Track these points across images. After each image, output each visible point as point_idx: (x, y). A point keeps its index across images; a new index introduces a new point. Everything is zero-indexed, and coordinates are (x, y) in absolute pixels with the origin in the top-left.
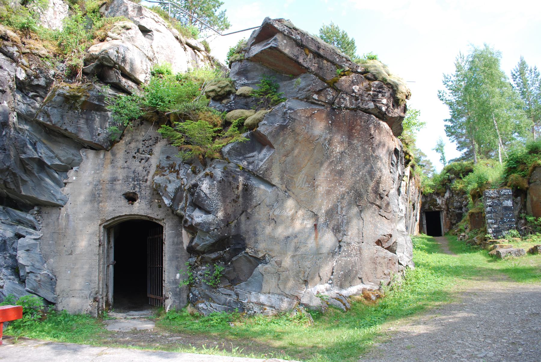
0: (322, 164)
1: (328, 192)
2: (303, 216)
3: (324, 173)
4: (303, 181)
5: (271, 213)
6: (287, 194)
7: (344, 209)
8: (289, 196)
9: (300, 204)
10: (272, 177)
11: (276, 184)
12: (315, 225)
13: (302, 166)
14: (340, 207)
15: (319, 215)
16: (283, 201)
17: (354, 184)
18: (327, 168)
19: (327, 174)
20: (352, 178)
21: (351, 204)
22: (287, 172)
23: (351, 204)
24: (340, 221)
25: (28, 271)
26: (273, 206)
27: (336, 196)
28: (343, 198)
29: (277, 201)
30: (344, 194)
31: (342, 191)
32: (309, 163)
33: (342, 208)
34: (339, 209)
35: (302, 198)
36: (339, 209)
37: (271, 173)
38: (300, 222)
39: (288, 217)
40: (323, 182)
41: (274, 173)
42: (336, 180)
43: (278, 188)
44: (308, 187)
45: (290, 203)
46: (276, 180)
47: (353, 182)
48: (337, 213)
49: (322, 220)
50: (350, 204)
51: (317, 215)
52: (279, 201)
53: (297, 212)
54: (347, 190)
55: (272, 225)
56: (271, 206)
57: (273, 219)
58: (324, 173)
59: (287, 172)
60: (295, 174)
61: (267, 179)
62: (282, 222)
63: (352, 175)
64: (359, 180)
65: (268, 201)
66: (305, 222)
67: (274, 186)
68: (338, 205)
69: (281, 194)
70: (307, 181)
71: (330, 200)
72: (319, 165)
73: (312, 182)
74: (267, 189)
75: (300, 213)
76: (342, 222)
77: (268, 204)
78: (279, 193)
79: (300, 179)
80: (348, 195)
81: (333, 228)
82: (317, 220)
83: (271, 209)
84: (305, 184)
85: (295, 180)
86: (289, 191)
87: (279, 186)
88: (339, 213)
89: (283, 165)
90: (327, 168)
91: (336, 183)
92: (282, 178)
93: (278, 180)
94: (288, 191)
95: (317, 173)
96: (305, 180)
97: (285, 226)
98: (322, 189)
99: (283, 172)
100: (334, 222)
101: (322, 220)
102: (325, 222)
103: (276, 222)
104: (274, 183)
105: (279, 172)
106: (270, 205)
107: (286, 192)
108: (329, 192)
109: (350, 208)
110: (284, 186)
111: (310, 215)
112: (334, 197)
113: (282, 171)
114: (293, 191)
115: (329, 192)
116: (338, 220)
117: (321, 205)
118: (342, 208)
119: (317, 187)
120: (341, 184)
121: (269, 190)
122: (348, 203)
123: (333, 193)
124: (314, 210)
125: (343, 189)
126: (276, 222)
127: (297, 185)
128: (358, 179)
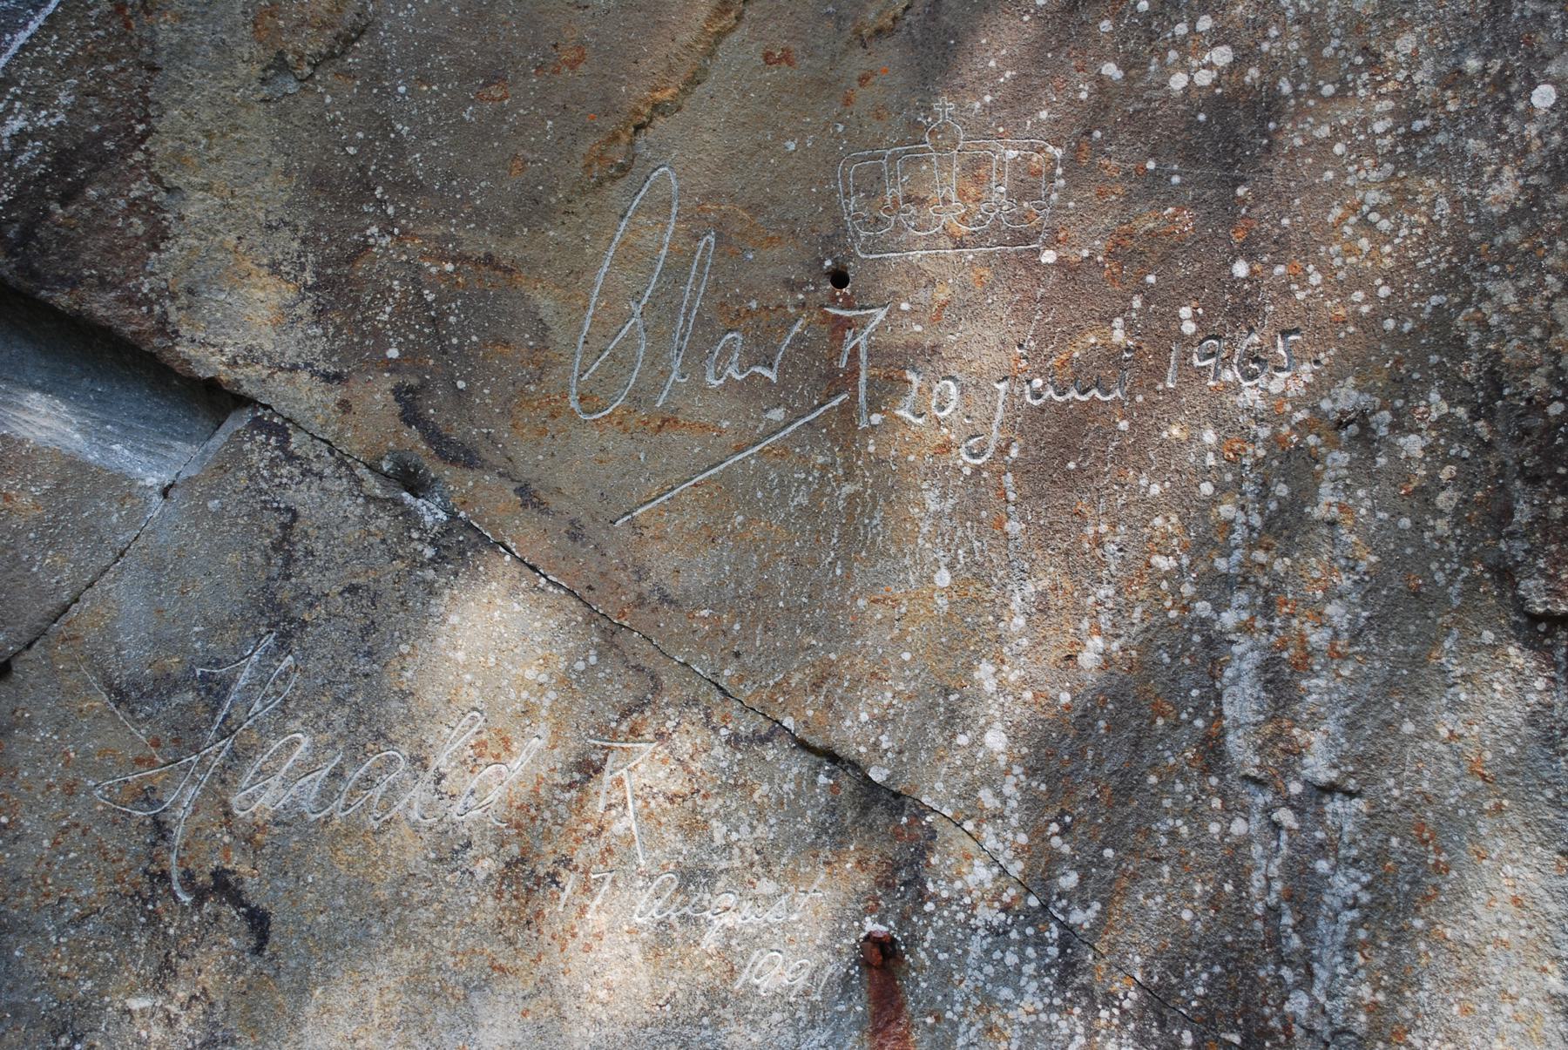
0: (935, 50)
1: (1061, 451)
2: (693, 827)
3: (975, 169)
4: (664, 307)
5: (183, 801)
6: (431, 513)
7: (1316, 687)
8: (462, 546)
9: (630, 652)
10: (166, 266)
11: (248, 379)
12: (881, 962)
13: (634, 94)
14: (1245, 657)
15: (936, 794)
16: (379, 623)
17: (1450, 280)
18: (1019, 99)
19: (1026, 187)
20: (1403, 199)
21: (1421, 599)
22: (408, 187)
23: (1421, 599)
24: (1266, 877)
25: (1325, 775)
26: (214, 689)
27: (1182, 498)
28: (1286, 526)
29: (286, 629)
30: (1296, 464)
31: (1273, 415)
32: (741, 49)
33: (1280, 681)
34: (1242, 702)
35: (663, 563)
36: (1242, 702)
37: (149, 209)
38: (645, 908)
39: (451, 850)
40: (969, 309)
41: (196, 207)
42: (1165, 249)
43: (280, 430)
44: (751, 390)
45: (491, 640)
46: (246, 320)
47: (1436, 260)
48: (1212, 752)
49: (976, 871)
50: (1401, 606)
51: (896, 800)
52: (325, 629)
53: (588, 769)
54: (1347, 396)
55: (209, 968)
56: (188, 703)
57: (224, 886)
58: (975, 169)
59: (408, 187)
60: (534, 208)
61: (101, 306)
62: (372, 918)
63: (1414, 149)
64: (1528, 209)
65: (125, 618)
66: (728, 913)
67: (215, 400)
68: (1215, 644)
69: (329, 506)
70: (726, 312)
71: (1081, 567)
72: (889, 55)
73: (810, 324)
74: (122, 455)
75: (643, 772)
76: (1303, 891)
77: (133, 654)
78: (302, 496)
79: (618, 281)
80: (1363, 471)
81: (1158, 1001)
82: (904, 877)
83: (185, 737)
84: (697, 355)
85: (545, 302)
86: (466, 458)
87: (303, 397)
88: (1241, 750)
89: (332, 95)
90: (1019, 99)
91: (1163, 301)
92: (335, 289)
93: (285, 319)
94: (440, 472)
95: (871, 186)
96: (693, 294)
97: (415, 983)
98: (963, 398)
99: (339, 194)
100: (1167, 906)
101: (976, 871)
102: (1033, 910)
103: (259, 922)
104: (212, 364)
105: (271, 193)
106: (166, 685)
107: (411, 480)
108: (1065, 446)
109: (1410, 680)
110: (378, 394)
111: (789, 808)
112: (1143, 522)
113: (320, 181)
114: (531, 460)
115: (1065, 446)
116: (1234, 862)
117: (965, 635)
118: (1280, 681)
119: (888, 387)
120: (1244, 311)
121: (151, 464)
122: (1370, 587)
123: (1134, 453)
124: (853, 730)
125: (1275, 386)
126: (259, 922)
127: (577, 371)
128: (1505, 189)
